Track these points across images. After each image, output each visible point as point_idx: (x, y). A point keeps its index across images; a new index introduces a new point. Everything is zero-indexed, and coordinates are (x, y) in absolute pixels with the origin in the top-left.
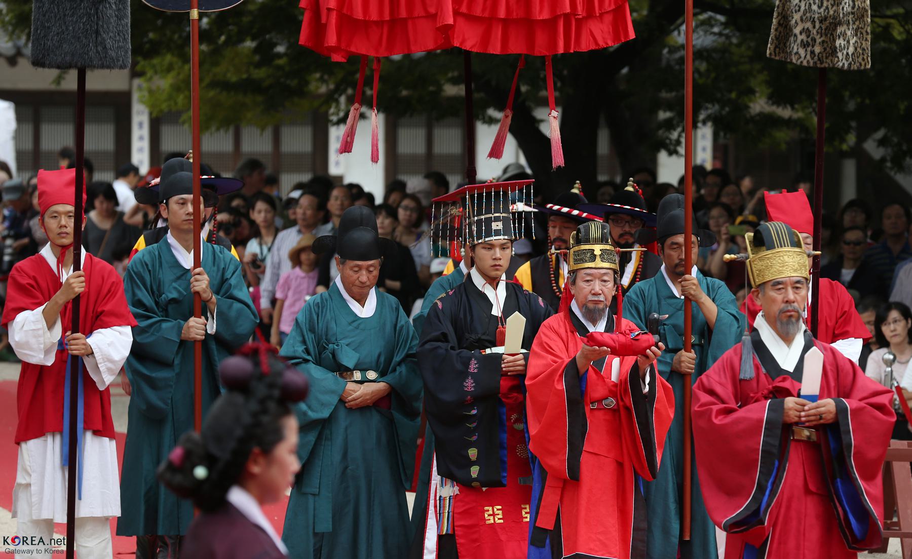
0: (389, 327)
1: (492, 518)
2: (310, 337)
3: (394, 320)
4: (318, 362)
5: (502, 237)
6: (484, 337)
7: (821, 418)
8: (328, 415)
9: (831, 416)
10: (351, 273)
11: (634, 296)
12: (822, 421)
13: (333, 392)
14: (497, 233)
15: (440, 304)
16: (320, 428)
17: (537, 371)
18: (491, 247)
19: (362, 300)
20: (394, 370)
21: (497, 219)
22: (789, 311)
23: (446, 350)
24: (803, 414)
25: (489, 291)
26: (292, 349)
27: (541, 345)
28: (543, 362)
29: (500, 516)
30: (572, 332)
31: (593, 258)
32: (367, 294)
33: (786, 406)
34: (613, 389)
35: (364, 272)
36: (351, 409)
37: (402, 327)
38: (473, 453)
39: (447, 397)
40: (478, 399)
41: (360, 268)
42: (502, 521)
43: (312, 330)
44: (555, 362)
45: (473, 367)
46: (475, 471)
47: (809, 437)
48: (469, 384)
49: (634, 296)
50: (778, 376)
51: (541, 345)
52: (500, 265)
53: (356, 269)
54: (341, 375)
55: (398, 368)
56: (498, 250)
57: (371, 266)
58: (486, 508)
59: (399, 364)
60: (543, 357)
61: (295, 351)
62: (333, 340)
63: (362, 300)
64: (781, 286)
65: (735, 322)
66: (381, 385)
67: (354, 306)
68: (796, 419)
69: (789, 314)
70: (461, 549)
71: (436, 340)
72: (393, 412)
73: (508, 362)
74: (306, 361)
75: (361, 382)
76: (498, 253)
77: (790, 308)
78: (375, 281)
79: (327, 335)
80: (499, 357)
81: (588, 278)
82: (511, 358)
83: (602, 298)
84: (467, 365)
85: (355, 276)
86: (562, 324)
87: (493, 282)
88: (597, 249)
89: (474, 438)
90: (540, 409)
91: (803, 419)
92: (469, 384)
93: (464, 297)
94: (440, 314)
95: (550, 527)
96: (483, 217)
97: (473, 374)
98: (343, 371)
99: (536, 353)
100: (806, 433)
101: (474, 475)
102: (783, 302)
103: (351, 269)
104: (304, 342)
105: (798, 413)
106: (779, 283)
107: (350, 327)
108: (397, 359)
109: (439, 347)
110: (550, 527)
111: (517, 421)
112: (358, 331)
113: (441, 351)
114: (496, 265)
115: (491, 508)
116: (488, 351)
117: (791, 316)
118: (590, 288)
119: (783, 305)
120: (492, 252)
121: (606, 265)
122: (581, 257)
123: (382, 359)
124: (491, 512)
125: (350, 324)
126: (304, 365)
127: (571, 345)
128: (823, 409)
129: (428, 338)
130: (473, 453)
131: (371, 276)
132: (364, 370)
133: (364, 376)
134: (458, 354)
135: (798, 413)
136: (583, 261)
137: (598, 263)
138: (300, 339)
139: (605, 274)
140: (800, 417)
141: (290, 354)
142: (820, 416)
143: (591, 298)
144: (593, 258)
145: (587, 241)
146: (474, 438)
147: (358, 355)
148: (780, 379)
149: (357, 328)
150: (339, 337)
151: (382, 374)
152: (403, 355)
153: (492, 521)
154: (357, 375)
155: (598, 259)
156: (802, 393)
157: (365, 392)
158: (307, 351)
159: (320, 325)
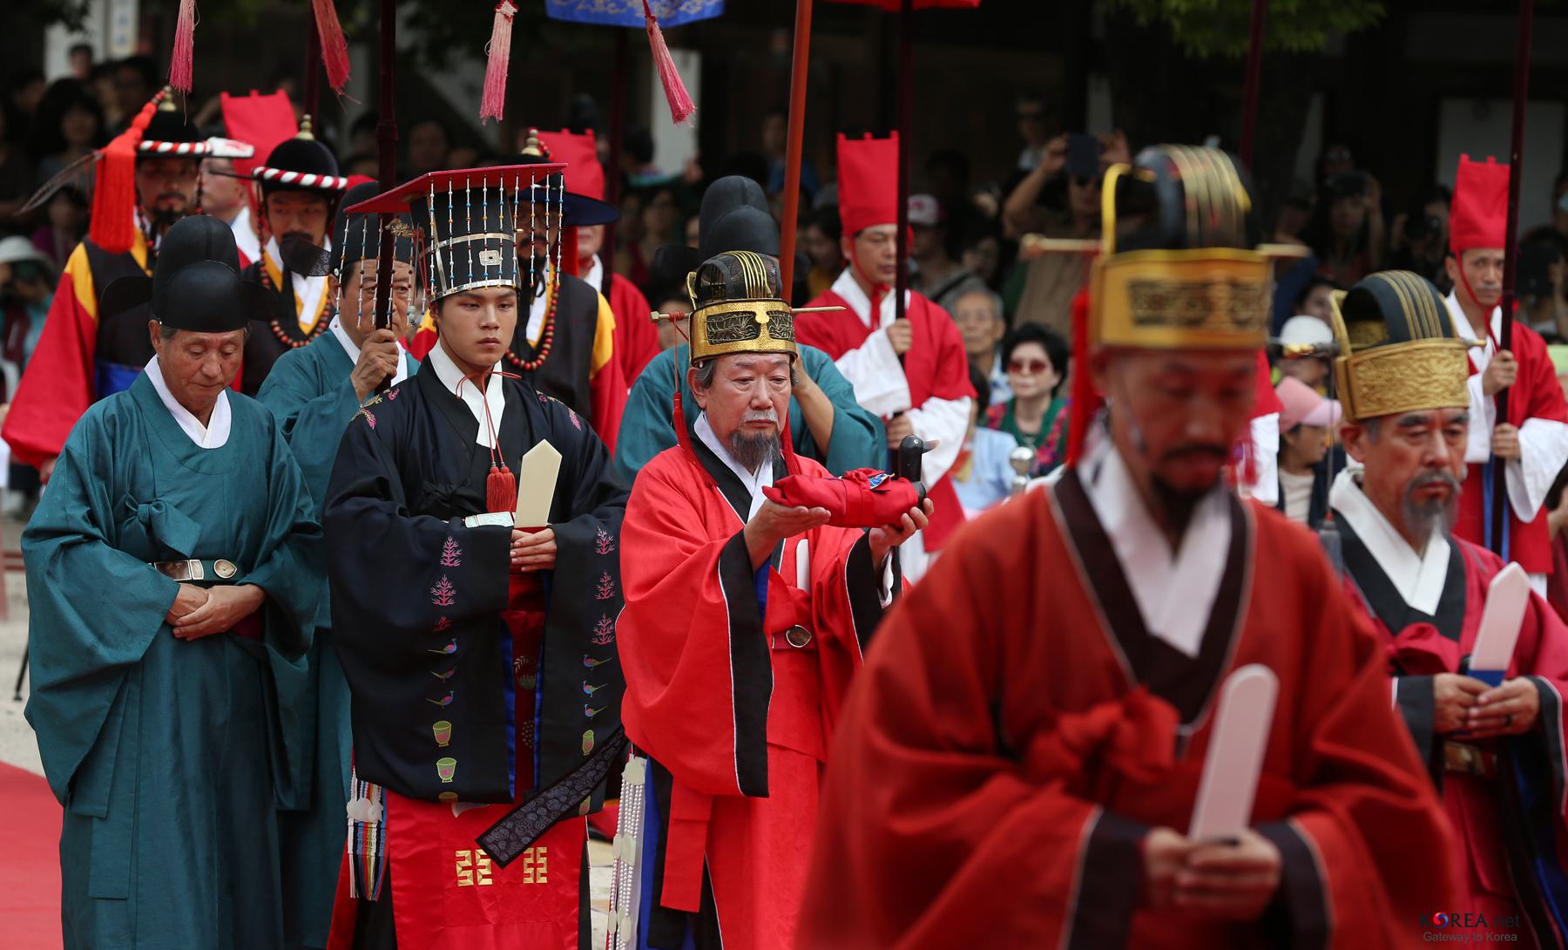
0: (258, 467)
1: (469, 873)
2: (95, 487)
3: (266, 451)
4: (115, 542)
5: (498, 282)
6: (463, 491)
7: (1509, 723)
8: (140, 654)
9: (1528, 719)
10: (186, 357)
11: (659, 380)
12: (1508, 730)
13: (151, 606)
14: (493, 272)
15: (370, 418)
16: (121, 679)
17: (653, 570)
18: (477, 301)
19: (203, 413)
20: (268, 558)
21: (493, 245)
22: (1434, 485)
23: (391, 515)
24: (1474, 711)
25: (471, 396)
26: (61, 514)
27: (649, 517)
28: (665, 551)
29: (486, 872)
30: (710, 487)
31: (754, 330)
32: (214, 400)
33: (1438, 694)
34: (804, 606)
35: (214, 355)
36: (183, 642)
37: (283, 466)
38: (442, 731)
39: (402, 617)
40: (461, 623)
41: (206, 346)
42: (488, 882)
43: (102, 472)
44: (690, 551)
45: (451, 554)
46: (446, 769)
47: (1471, 765)
48: (444, 592)
49: (659, 380)
50: (1404, 624)
51: (649, 517)
52: (495, 341)
53: (197, 349)
54: (162, 568)
55: (276, 553)
56: (491, 308)
57: (229, 342)
58: (460, 853)
59: (278, 545)
60: (659, 542)
61: (67, 518)
62: (147, 494)
63: (203, 413)
64: (1420, 428)
65: (866, 432)
66: (249, 590)
67: (189, 424)
68: (1458, 724)
69: (1432, 490)
70: (402, 938)
71: (367, 492)
72: (268, 646)
73: (522, 546)
74: (91, 539)
75: (206, 584)
76: (492, 314)
77: (1437, 479)
78: (233, 375)
79: (133, 485)
80: (502, 537)
81: (746, 374)
82: (529, 537)
83: (772, 416)
84: (436, 550)
85: (196, 363)
86: (686, 471)
87: (478, 375)
88: (761, 311)
89: (447, 701)
90: (662, 653)
91: (1473, 723)
92: (444, 592)
93: (419, 403)
94: (373, 441)
95: (693, 905)
96: (469, 238)
97: (450, 571)
98: (167, 559)
99: (638, 536)
100: (1465, 755)
101: (447, 778)
102: (1422, 462)
103: (187, 348)
104: (85, 498)
105: (1461, 711)
106: (1418, 421)
107: (182, 470)
108: (276, 533)
109: (374, 508)
110: (693, 905)
111: (526, 670)
112: (199, 477)
113: (377, 517)
114: (487, 341)
115: (467, 853)
116: (471, 522)
117: (1435, 496)
118: (749, 394)
119: (1422, 470)
120: (479, 313)
121: (780, 345)
122: (723, 329)
123: (244, 535)
124: (468, 863)
125: (182, 461)
126: (87, 549)
127: (712, 516)
128: (1514, 702)
129: (350, 488)
130: (442, 731)
131: (227, 365)
132: (207, 558)
133: (209, 571)
134: (416, 525)
135: (1461, 711)
136: (732, 336)
137: (764, 341)
138: (75, 491)
139: (779, 364)
140: (1466, 718)
141: (57, 522)
142: (1507, 715)
143: (750, 415)
144: (754, 330)
145: (740, 293)
146: (447, 701)
147: (199, 527)
148: (1409, 630)
149: (196, 470)
150: (160, 488)
151: (246, 567)
152: (286, 527)
153: (470, 882)
154: (196, 570)
155: (764, 332)
156: (1474, 662)
157: (219, 607)
158: (92, 518)
159: (119, 464)
